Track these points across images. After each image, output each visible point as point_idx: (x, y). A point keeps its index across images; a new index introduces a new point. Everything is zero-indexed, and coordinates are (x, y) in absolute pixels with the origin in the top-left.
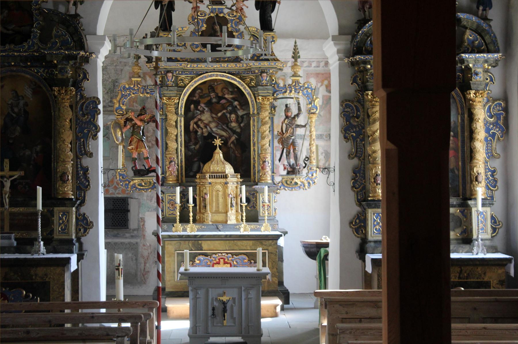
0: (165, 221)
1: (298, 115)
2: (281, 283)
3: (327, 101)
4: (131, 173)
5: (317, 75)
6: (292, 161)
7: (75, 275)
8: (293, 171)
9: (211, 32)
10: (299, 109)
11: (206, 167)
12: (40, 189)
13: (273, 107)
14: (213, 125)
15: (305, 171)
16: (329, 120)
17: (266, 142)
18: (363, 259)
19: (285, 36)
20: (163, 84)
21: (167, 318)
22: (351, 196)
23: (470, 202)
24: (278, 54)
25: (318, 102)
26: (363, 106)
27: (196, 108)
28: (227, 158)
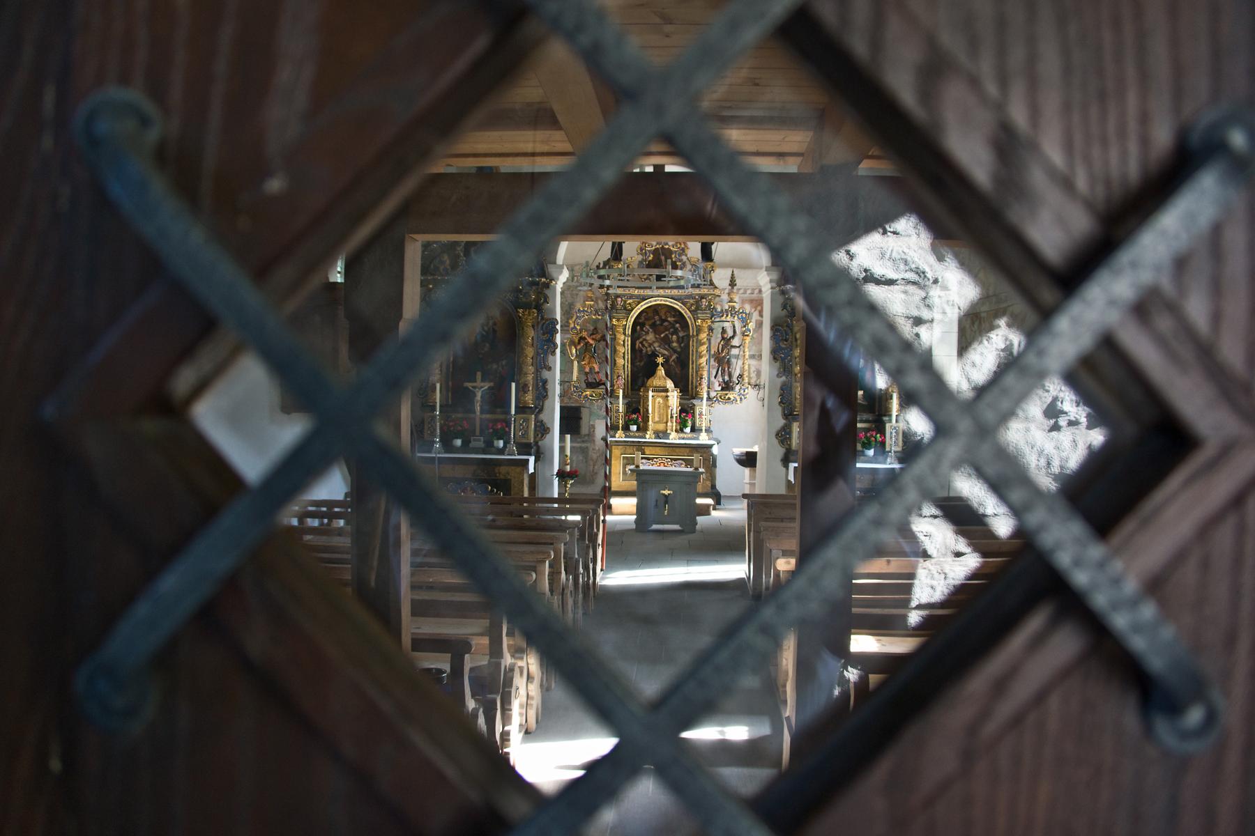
0: (612, 428)
1: (733, 337)
2: (713, 486)
3: (760, 325)
4: (584, 385)
5: (751, 301)
6: (727, 378)
7: (533, 477)
8: (727, 387)
9: (655, 264)
10: (735, 332)
11: (649, 382)
12: (513, 385)
13: (711, 329)
14: (656, 345)
15: (738, 387)
16: (760, 343)
17: (703, 360)
18: (787, 467)
19: (724, 265)
20: (613, 306)
21: (611, 514)
22: (778, 411)
23: (885, 419)
24: (716, 282)
25: (751, 326)
26: (792, 330)
27: (642, 329)
28: (668, 374)
